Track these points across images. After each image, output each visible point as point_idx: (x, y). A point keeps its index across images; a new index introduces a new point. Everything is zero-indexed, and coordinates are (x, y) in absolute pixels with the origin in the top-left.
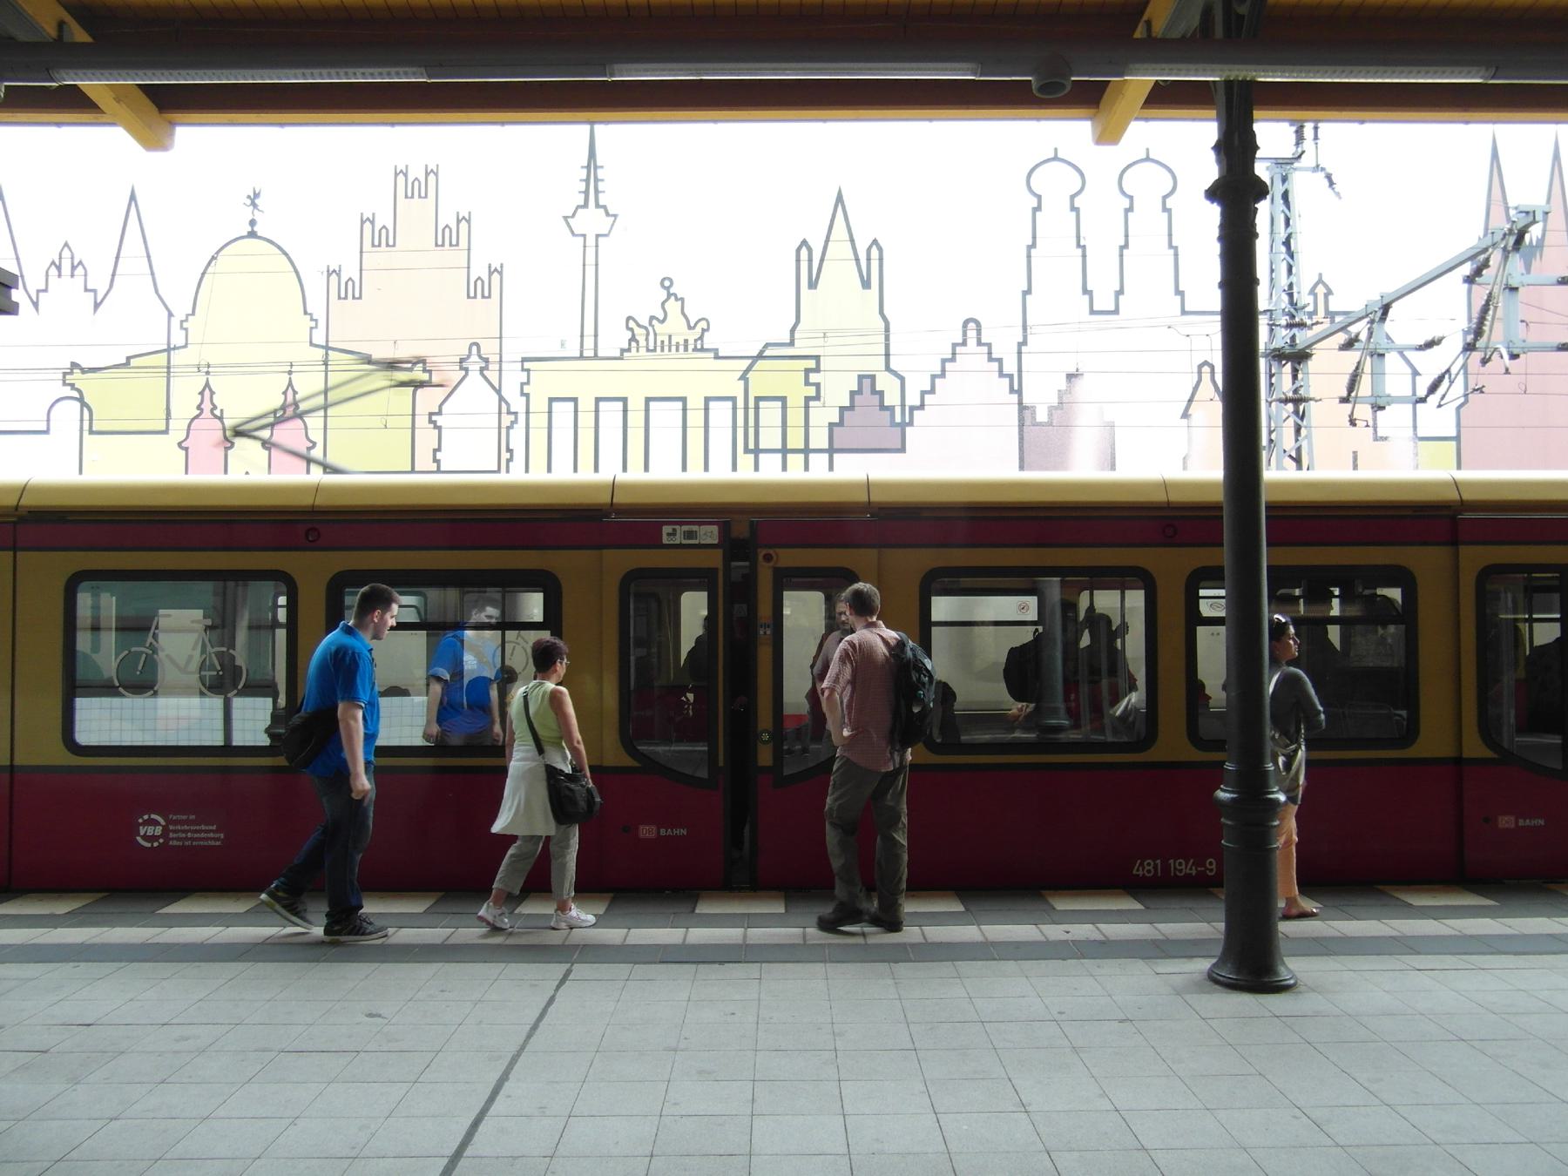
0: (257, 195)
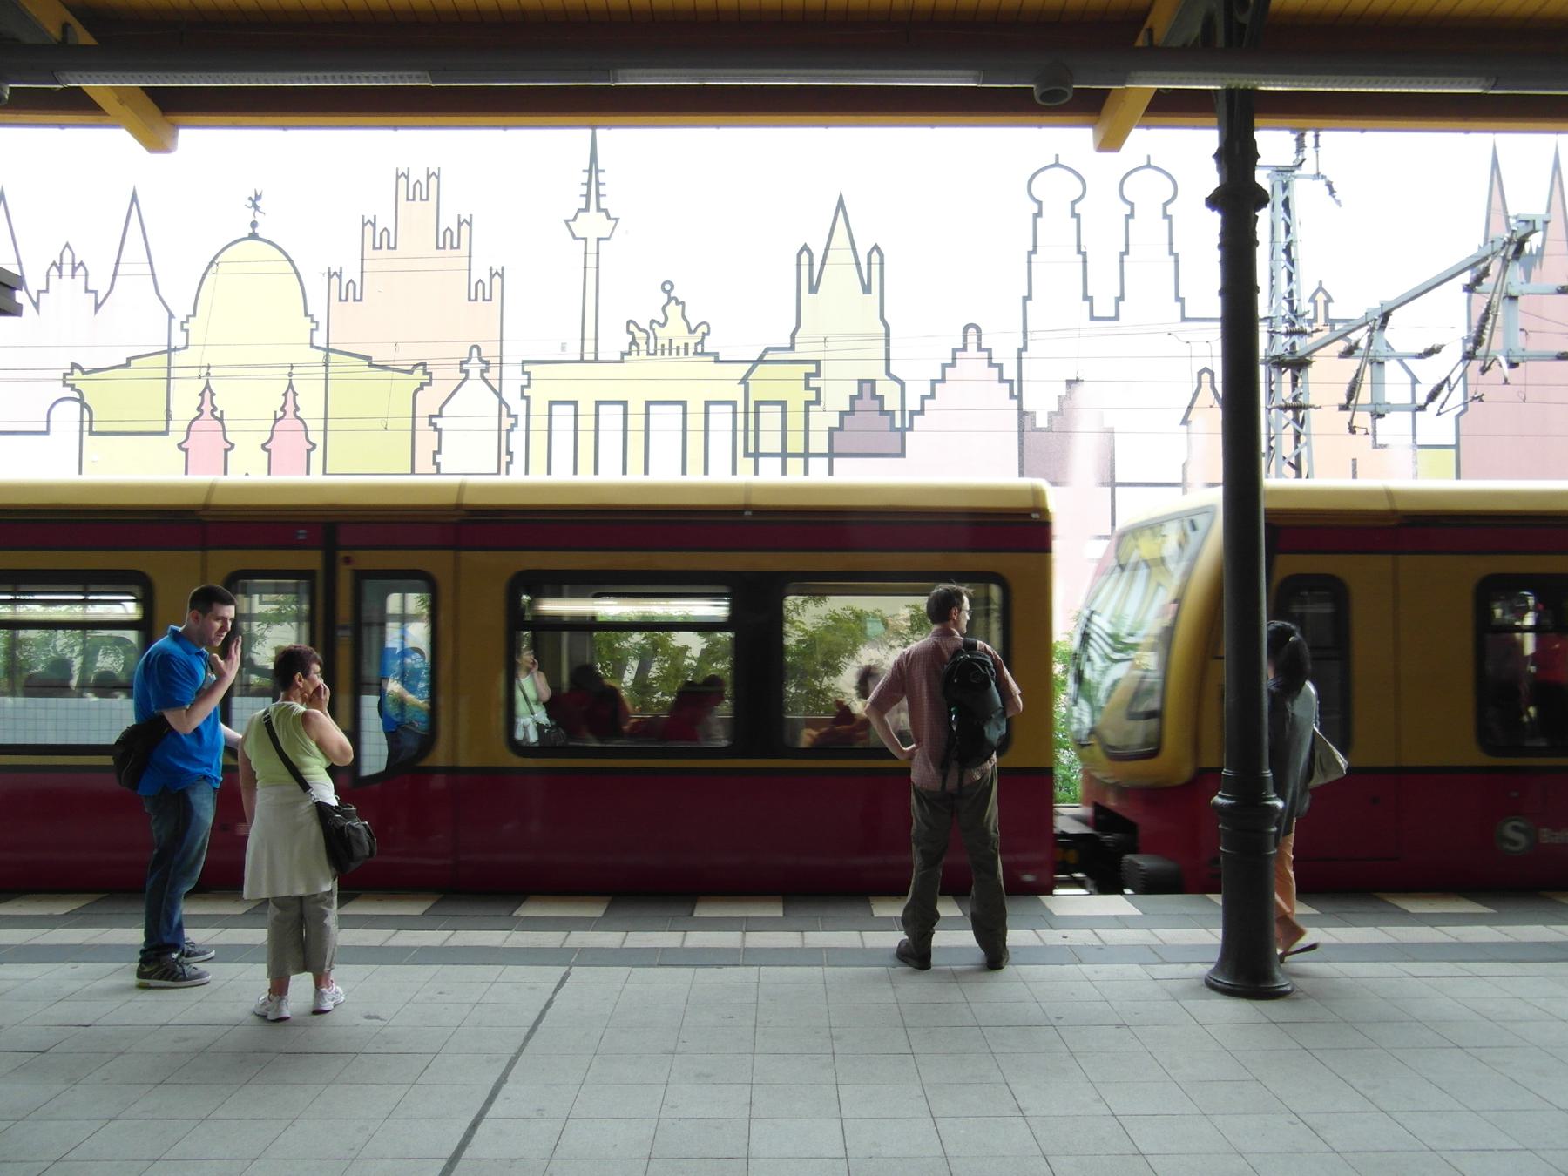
0: (258, 197)
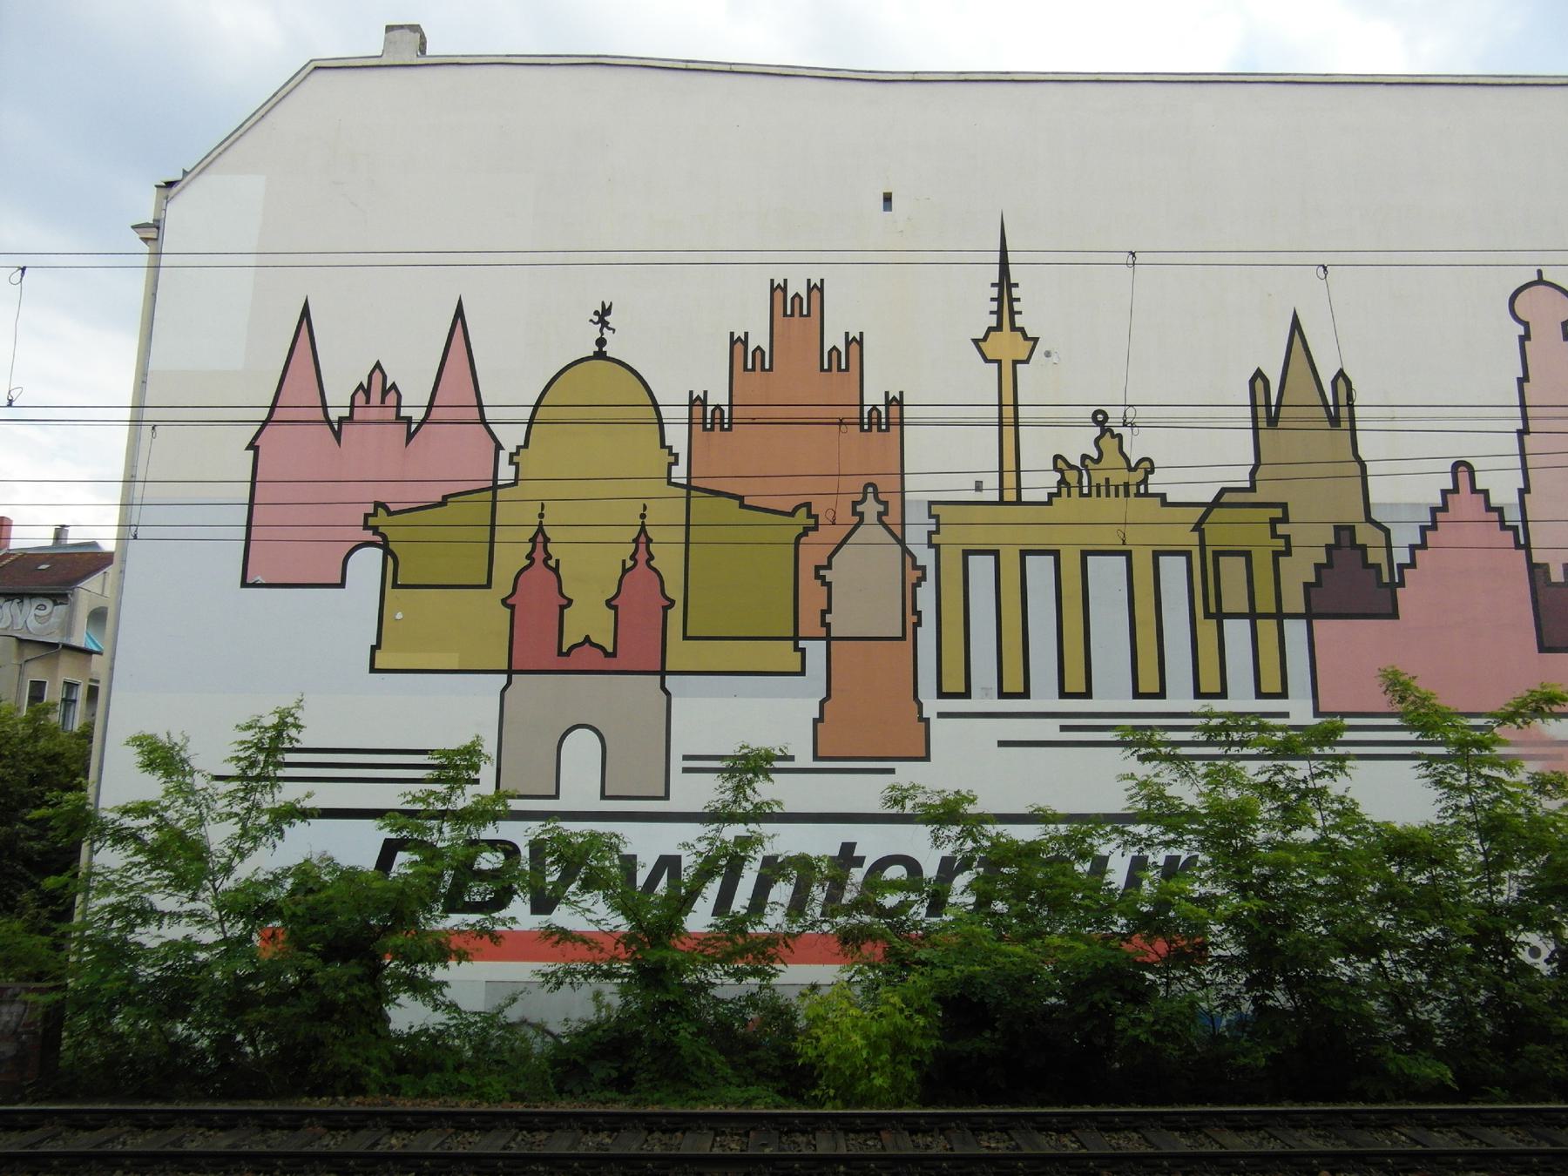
0: (606, 311)
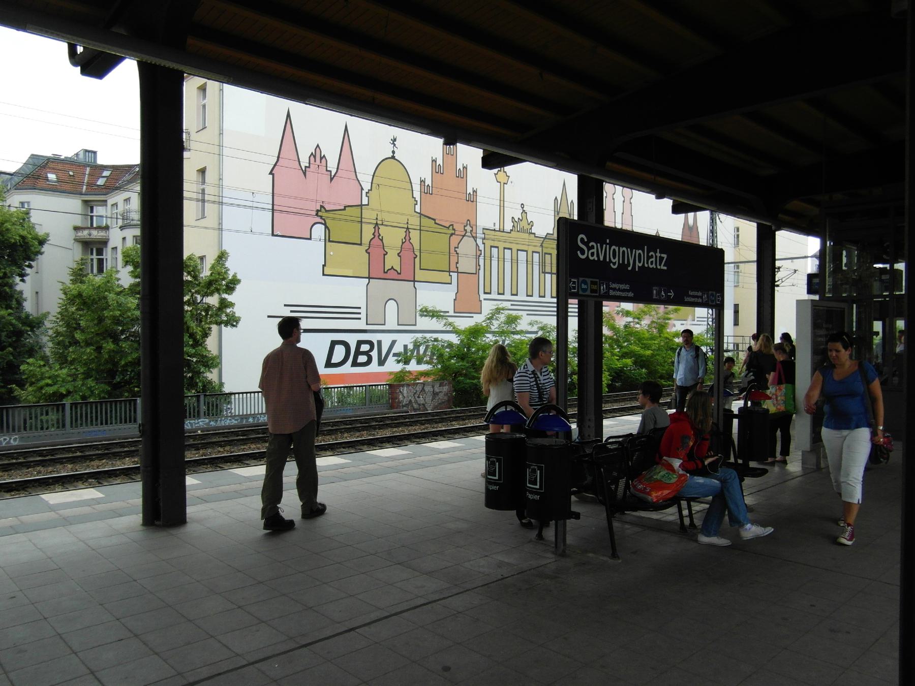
0: (395, 140)
